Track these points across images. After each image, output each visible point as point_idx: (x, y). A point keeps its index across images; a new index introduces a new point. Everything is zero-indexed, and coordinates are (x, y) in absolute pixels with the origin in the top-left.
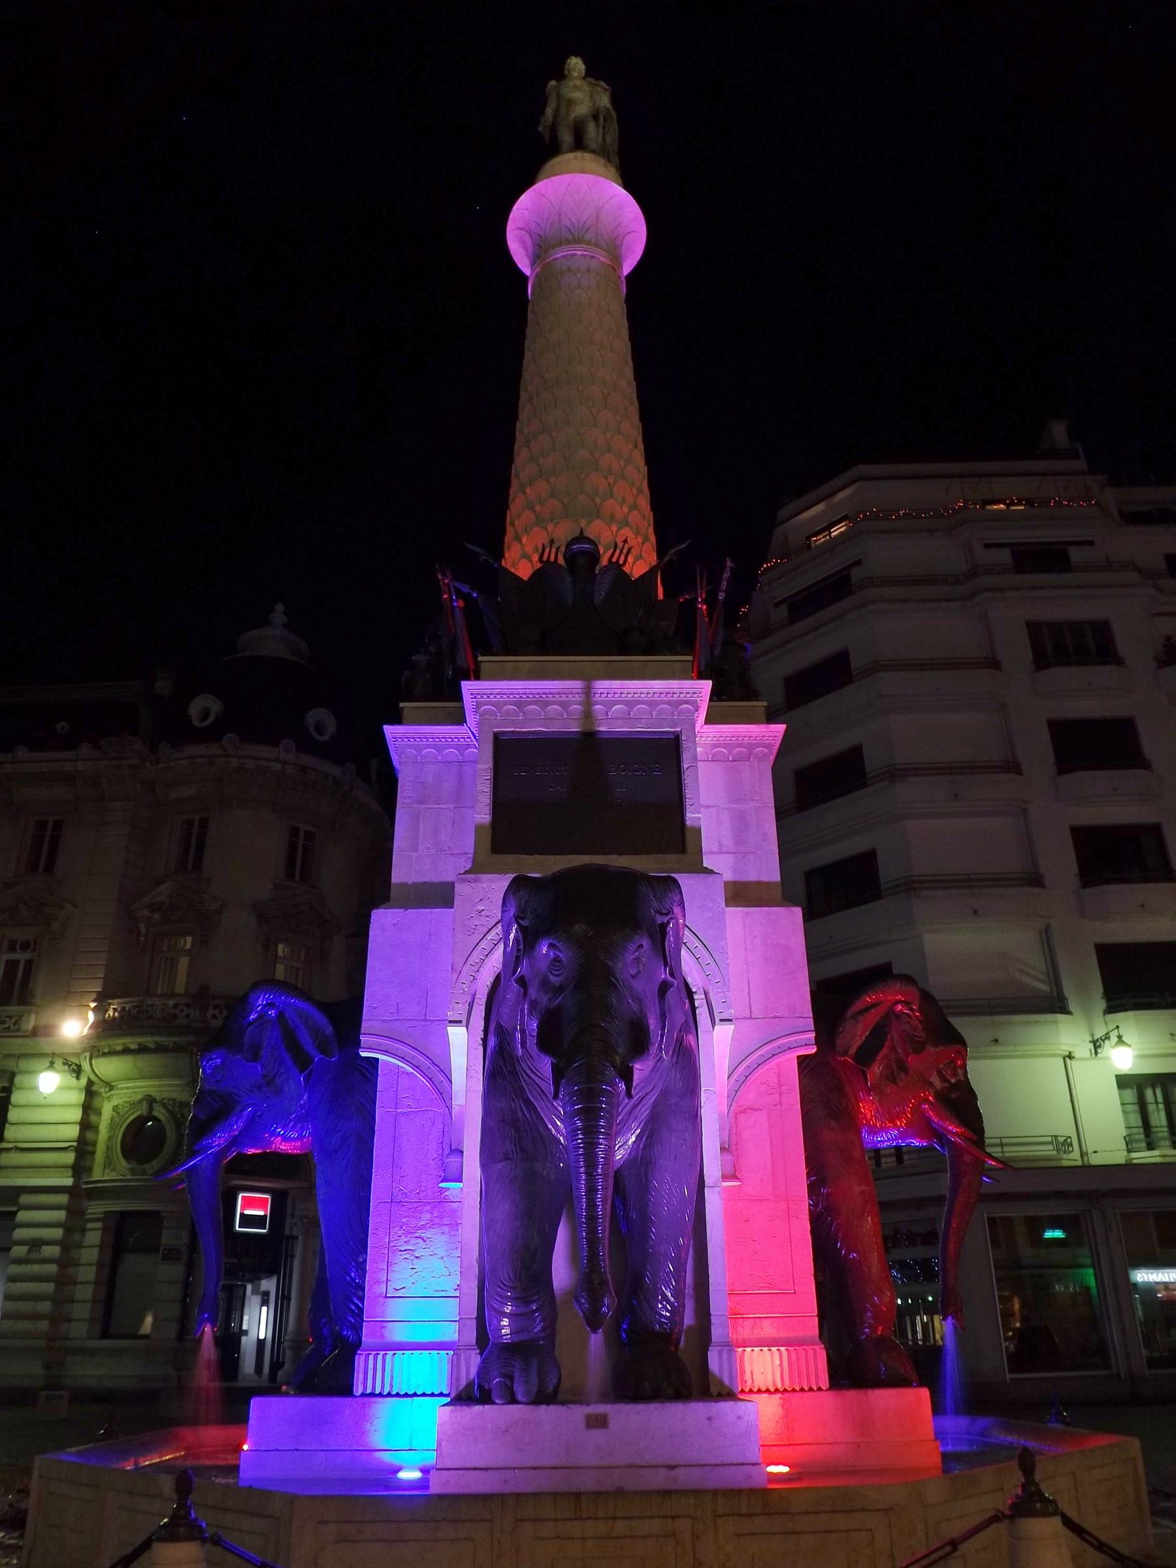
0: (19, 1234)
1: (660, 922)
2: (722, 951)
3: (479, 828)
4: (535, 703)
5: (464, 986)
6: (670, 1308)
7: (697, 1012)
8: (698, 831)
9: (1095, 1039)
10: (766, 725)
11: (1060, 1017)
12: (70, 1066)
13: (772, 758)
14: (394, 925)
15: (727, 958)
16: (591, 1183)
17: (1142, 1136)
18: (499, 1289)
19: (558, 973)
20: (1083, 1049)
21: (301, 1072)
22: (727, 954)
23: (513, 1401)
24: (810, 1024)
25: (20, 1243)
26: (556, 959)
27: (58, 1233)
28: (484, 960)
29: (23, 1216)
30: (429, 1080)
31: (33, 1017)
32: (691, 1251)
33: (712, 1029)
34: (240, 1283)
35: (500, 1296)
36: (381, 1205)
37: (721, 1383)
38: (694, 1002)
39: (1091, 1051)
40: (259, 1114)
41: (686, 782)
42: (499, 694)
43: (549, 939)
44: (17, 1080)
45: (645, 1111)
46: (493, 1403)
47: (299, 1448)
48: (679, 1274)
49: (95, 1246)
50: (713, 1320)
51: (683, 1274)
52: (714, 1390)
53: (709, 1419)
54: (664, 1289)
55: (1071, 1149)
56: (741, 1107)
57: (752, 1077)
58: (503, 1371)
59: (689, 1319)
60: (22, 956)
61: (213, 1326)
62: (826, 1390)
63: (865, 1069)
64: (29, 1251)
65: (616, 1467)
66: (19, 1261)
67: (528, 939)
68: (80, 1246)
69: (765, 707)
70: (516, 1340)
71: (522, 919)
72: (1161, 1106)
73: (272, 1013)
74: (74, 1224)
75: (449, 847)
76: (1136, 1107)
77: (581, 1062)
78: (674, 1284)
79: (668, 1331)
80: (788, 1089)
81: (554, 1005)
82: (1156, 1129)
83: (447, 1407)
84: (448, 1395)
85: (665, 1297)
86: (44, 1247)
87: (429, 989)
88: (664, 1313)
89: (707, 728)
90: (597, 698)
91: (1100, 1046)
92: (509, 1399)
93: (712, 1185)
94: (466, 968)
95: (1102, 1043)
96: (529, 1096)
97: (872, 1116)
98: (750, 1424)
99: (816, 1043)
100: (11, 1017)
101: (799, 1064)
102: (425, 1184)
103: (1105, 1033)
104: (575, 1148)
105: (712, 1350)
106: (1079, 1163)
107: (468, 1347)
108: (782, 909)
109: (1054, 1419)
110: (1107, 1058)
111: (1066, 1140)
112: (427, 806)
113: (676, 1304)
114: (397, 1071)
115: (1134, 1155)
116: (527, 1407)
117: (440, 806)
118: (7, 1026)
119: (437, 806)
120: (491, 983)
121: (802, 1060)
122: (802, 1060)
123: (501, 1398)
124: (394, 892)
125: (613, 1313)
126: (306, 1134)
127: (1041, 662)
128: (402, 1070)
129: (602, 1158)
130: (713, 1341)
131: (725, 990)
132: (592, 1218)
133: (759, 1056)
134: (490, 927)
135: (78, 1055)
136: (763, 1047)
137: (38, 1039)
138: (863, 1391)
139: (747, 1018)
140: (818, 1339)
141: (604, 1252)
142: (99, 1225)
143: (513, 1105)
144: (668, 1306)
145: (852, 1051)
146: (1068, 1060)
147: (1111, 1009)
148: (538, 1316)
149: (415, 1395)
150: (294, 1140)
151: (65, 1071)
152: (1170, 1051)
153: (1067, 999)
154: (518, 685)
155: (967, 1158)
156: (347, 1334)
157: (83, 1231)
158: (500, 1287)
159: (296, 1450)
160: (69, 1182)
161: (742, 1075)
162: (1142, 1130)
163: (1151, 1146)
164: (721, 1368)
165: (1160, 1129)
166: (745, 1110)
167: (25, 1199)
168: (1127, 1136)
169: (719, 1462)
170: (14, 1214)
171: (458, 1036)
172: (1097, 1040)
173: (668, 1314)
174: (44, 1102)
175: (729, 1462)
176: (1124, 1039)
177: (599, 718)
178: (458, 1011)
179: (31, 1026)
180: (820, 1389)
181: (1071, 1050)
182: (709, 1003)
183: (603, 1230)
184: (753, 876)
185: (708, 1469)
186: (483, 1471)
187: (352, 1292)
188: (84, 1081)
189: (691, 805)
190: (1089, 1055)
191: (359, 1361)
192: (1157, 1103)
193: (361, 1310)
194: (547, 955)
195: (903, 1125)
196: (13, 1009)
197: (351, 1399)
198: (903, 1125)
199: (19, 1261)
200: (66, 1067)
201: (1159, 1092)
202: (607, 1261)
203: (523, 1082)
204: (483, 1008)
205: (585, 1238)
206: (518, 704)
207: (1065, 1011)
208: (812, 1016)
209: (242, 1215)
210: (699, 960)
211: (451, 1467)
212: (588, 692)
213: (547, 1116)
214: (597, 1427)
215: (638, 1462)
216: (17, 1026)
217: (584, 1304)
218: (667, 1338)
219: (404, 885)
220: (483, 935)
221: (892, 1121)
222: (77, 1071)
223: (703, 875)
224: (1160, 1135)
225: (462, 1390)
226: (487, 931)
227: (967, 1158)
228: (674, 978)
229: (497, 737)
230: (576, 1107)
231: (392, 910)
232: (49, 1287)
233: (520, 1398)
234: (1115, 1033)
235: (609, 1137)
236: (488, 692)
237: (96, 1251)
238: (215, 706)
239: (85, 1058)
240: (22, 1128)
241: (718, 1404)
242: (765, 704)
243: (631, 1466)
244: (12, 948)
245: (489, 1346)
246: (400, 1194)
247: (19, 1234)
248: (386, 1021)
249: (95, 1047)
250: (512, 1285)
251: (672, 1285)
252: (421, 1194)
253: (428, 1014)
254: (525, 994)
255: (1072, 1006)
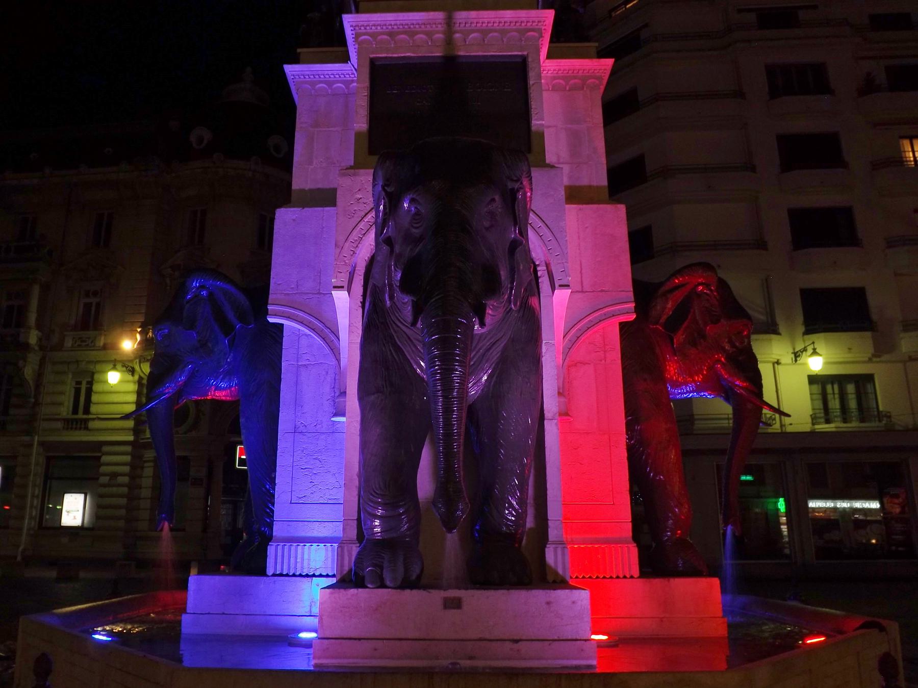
0: (103, 469)
1: (510, 187)
2: (562, 230)
3: (358, 135)
4: (405, 33)
5: (345, 259)
6: (515, 514)
7: (540, 281)
8: (541, 135)
9: (796, 351)
10: (597, 60)
11: (773, 336)
12: (127, 368)
13: (602, 88)
14: (294, 220)
15: (566, 236)
16: (447, 405)
17: (822, 415)
18: (371, 496)
19: (418, 225)
20: (787, 358)
21: (226, 337)
22: (566, 233)
23: (383, 586)
24: (631, 295)
25: (105, 475)
26: (418, 213)
27: (126, 469)
28: (362, 238)
29: (105, 459)
30: (322, 339)
31: (103, 338)
32: (532, 471)
33: (552, 295)
34: (241, 499)
35: (372, 502)
36: (286, 435)
37: (557, 573)
38: (537, 273)
39: (792, 359)
40: (196, 369)
41: (532, 95)
42: (374, 25)
43: (410, 194)
44: (96, 376)
45: (496, 355)
46: (367, 587)
47: (226, 613)
48: (523, 487)
49: (146, 477)
50: (550, 523)
51: (526, 487)
52: (550, 578)
53: (548, 603)
54: (510, 498)
55: (774, 422)
56: (573, 361)
57: (582, 338)
58: (374, 562)
59: (530, 523)
60: (94, 300)
61: (170, 523)
62: (637, 578)
63: (672, 335)
64: (110, 479)
65: (470, 640)
66: (104, 486)
67: (393, 202)
68: (141, 477)
69: (596, 47)
70: (386, 537)
71: (388, 186)
72: (837, 396)
73: (203, 294)
74: (136, 464)
75: (337, 161)
76: (820, 397)
77: (437, 298)
78: (518, 494)
79: (513, 531)
80: (610, 348)
81: (415, 254)
82: (832, 411)
83: (327, 590)
84: (334, 576)
85: (511, 505)
86: (119, 477)
87: (322, 270)
88: (510, 518)
89: (548, 63)
90: (456, 27)
91: (799, 356)
92: (379, 584)
93: (550, 418)
94: (347, 244)
95: (801, 354)
96: (397, 341)
97: (675, 373)
98: (583, 608)
99: (635, 312)
100: (89, 338)
101: (621, 329)
102: (321, 419)
103: (803, 347)
104: (433, 374)
105: (549, 547)
106: (779, 431)
107: (350, 542)
108: (609, 206)
109: (792, 598)
110: (805, 364)
111: (771, 416)
112: (321, 129)
113: (520, 511)
114: (298, 333)
115: (817, 427)
116: (394, 591)
117: (331, 129)
118: (87, 343)
119: (327, 129)
120: (368, 258)
121: (623, 326)
122: (623, 326)
123: (372, 583)
124: (294, 197)
125: (466, 516)
126: (233, 384)
127: (774, 93)
128: (302, 333)
129: (457, 383)
130: (550, 539)
131: (563, 261)
132: (448, 435)
133: (589, 321)
134: (367, 212)
135: (131, 361)
136: (592, 314)
137: (109, 351)
138: (667, 579)
139: (579, 292)
140: (631, 540)
141: (458, 465)
142: (151, 464)
143: (384, 349)
144: (513, 512)
145: (662, 321)
146: (776, 365)
147: (808, 331)
148: (404, 518)
149: (314, 576)
150: (224, 389)
151: (124, 371)
152: (846, 360)
153: (778, 325)
154: (389, 17)
155: (749, 406)
156: (264, 530)
157: (142, 468)
158: (372, 494)
159: (224, 614)
160: (131, 438)
161: (574, 340)
162: (822, 411)
163: (828, 421)
164: (556, 562)
165: (835, 411)
166: (576, 364)
167: (106, 449)
168: (813, 414)
169: (556, 638)
170: (100, 457)
171: (341, 298)
172: (797, 352)
173: (513, 518)
174: (112, 390)
175: (564, 638)
176: (817, 350)
177: (459, 44)
178: (343, 279)
179: (102, 344)
180: (632, 577)
181: (779, 358)
182: (550, 273)
183: (458, 447)
184: (585, 182)
185: (547, 643)
186: (357, 641)
187: (268, 500)
188: (136, 377)
189: (537, 114)
190: (790, 362)
191: (271, 550)
192: (834, 394)
193: (273, 511)
194: (409, 210)
195: (700, 379)
196: (91, 333)
197: (265, 578)
198: (700, 379)
199: (104, 486)
200: (124, 369)
201: (836, 387)
202: (462, 473)
203: (392, 330)
204: (362, 278)
205: (442, 452)
206: (391, 34)
207: (776, 332)
208: (632, 290)
209: (240, 458)
210: (542, 237)
211: (331, 637)
212: (449, 22)
213: (412, 358)
214: (454, 608)
215: (488, 637)
216: (93, 344)
217: (441, 508)
218: (513, 538)
219: (302, 191)
220: (361, 219)
221: (692, 376)
222: (132, 371)
223: (547, 169)
224: (835, 414)
225: (346, 574)
226: (364, 215)
227: (749, 406)
228: (523, 237)
229: (373, 62)
230: (433, 338)
231: (292, 209)
232: (123, 501)
233: (388, 583)
234: (812, 346)
235: (464, 365)
236: (365, 24)
237: (151, 480)
238: (207, 135)
239: (136, 363)
240: (100, 406)
241: (556, 591)
242: (596, 44)
243: (480, 640)
244: (87, 295)
245: (364, 541)
246: (301, 427)
247: (103, 469)
248: (288, 294)
249: (141, 356)
250: (382, 493)
251: (517, 496)
252: (318, 426)
253: (321, 289)
254: (392, 251)
255: (782, 329)
